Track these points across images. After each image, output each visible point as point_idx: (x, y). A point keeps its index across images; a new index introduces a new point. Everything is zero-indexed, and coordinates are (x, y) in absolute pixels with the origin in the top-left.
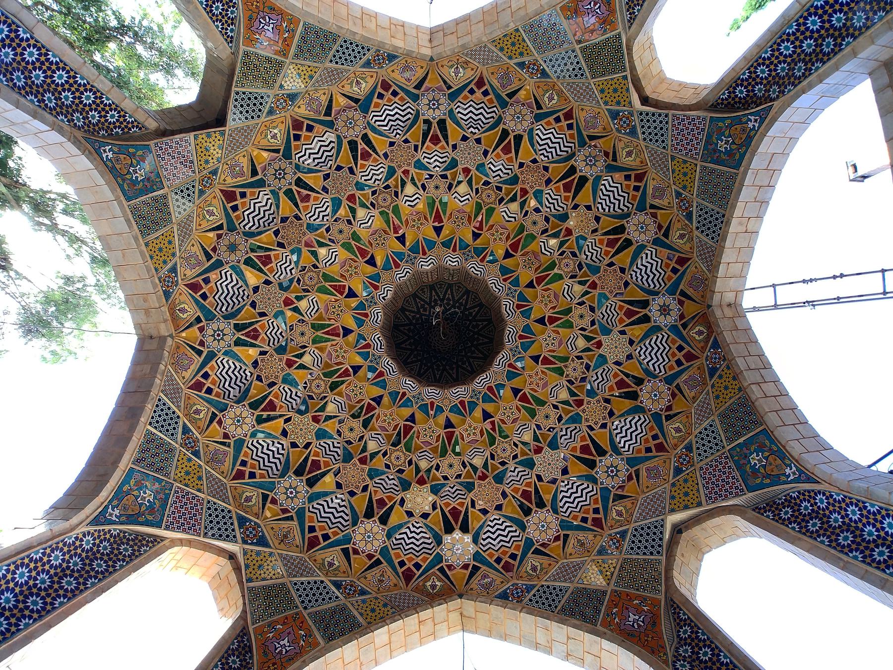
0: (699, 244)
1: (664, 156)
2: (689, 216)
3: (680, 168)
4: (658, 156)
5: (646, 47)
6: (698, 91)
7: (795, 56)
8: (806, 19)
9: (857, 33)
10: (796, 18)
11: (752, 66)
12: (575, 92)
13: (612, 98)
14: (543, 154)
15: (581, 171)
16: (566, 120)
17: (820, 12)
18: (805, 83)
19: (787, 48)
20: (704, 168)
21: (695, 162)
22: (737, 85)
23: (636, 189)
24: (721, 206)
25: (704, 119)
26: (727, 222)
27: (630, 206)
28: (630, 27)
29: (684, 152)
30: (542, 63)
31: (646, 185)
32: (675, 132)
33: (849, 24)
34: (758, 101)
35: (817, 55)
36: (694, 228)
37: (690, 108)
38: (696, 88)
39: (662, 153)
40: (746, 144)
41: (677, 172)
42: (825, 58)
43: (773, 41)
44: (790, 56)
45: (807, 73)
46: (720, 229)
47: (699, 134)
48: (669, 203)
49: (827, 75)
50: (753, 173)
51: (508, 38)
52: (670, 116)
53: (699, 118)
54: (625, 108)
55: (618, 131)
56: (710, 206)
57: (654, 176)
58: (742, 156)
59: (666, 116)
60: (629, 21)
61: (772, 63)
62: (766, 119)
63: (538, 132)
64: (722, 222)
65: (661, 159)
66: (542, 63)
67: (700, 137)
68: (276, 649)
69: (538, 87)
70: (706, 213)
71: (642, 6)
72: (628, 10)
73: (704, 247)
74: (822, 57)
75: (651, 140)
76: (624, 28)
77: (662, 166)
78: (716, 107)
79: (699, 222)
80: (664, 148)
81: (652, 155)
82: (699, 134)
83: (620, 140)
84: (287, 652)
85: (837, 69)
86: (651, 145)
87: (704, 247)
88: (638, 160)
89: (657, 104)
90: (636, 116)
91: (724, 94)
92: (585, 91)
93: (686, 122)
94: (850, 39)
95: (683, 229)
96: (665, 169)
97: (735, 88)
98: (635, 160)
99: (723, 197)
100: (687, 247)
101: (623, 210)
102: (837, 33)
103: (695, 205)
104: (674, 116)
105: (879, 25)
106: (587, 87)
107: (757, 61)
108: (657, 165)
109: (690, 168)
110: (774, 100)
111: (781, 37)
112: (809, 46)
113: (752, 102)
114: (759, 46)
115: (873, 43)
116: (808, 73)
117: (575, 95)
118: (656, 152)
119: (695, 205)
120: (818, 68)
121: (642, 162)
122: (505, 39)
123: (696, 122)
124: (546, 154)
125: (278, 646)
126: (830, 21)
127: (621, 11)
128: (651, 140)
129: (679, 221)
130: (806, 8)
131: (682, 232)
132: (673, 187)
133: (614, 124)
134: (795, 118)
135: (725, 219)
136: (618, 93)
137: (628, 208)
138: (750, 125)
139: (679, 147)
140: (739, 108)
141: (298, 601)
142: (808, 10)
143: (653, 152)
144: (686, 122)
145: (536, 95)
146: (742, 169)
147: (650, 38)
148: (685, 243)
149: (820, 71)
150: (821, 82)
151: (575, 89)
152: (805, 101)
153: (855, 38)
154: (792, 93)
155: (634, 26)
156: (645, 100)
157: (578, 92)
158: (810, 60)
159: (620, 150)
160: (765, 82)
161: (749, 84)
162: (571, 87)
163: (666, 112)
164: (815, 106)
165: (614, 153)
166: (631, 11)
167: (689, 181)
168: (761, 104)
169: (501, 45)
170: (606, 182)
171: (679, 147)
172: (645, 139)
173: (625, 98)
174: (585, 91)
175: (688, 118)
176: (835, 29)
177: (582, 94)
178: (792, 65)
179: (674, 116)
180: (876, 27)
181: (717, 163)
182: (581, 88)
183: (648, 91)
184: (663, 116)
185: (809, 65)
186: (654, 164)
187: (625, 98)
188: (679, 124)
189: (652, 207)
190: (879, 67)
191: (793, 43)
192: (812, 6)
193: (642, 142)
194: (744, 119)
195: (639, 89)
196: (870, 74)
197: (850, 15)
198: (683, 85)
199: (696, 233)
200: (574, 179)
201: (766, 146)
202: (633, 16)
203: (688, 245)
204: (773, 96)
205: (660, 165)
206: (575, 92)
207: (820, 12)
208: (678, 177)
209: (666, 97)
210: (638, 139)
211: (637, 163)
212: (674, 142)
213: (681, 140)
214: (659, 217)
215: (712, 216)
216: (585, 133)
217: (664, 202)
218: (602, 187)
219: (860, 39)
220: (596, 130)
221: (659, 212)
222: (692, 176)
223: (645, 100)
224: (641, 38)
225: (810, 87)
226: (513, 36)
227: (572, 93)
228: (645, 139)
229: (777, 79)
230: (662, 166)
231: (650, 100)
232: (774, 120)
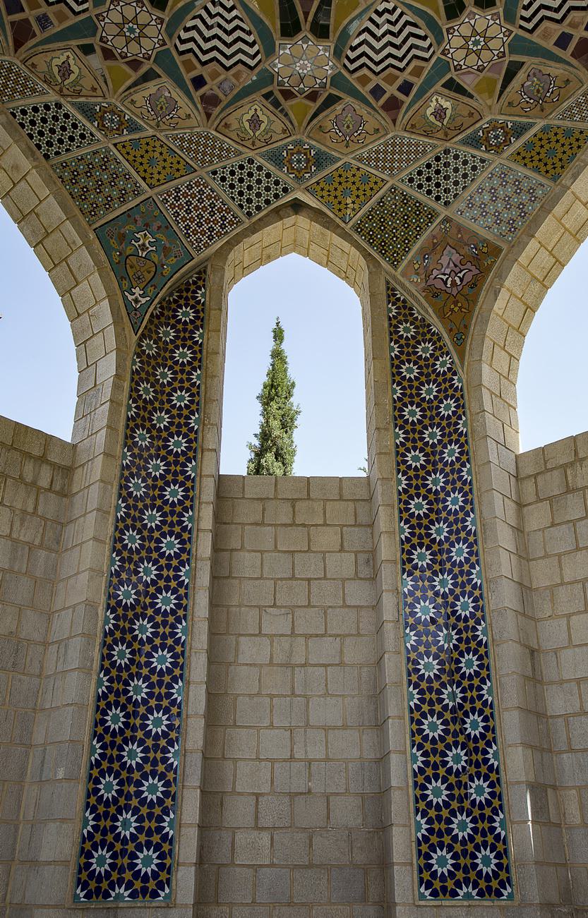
0: (30, 84)
1: (203, 161)
2: (87, 111)
3: (167, 164)
4: (212, 155)
5: (350, 271)
6: (239, 270)
7: (165, 398)
8: (175, 656)
9: (126, 473)
10: (200, 434)
11: (201, 351)
12: (405, 149)
13: (342, 180)
14: (391, 12)
15: (305, 40)
16: (393, 98)
17: (171, 619)
18: (127, 385)
19: (181, 399)
20: (137, 192)
21: (157, 190)
22: (197, 318)
23: (199, 82)
24: (64, 166)
25: (199, 249)
26: (33, 154)
27: (182, 48)
28: (388, 283)
29: (183, 189)
30: (485, 156)
31: (191, 98)
32: (218, 204)
33: (143, 473)
34: (156, 321)
35: (143, 419)
36: (62, 101)
37: (230, 245)
38: (246, 270)
39: (211, 162)
40: (122, 270)
41: (165, 156)
42: (132, 424)
43: (202, 394)
44: (170, 395)
45: (134, 395)
46: (31, 136)
47: (188, 227)
48: (133, 102)
49: (113, 412)
50: (74, 242)
51: (565, 157)
52: (244, 218)
53: (207, 246)
54: (314, 180)
55: (299, 143)
56: (77, 153)
57: (192, 122)
58: (107, 250)
59: (249, 214)
60: (393, 289)
61: (182, 371)
62: (128, 314)
63: (425, 44)
64: (39, 147)
65: (204, 154)
66: (485, 156)
67: (182, 225)
68: (445, 283)
69: (471, 115)
70: (72, 139)
71: (390, 319)
72: (404, 301)
73: (19, 88)
74: (139, 420)
75: (242, 167)
76: (394, 278)
77: (193, 147)
78: (199, 273)
79: (66, 116)
80: (215, 173)
81: (221, 149)
82: (188, 227)
83: (284, 131)
84: (461, 280)
85: (109, 427)
86: (235, 161)
87: (19, 88)
88: (235, 126)
89: (278, 214)
90: (289, 181)
91: (204, 295)
92: (393, 161)
93: (217, 228)
94: (137, 366)
95: (76, 83)
96: (186, 144)
97: (197, 312)
98: (240, 120)
99: (74, 180)
100: (40, 61)
101: (187, 30)
102: (145, 454)
103: (98, 135)
104: (240, 222)
105: (114, 502)
106: (392, 169)
107: (200, 361)
108: (202, 141)
109: (156, 176)
110: (140, 339)
111: (198, 404)
112: (160, 420)
113: (162, 314)
114: (216, 378)
115: (102, 481)
116: (134, 395)
117: (402, 145)
118: (220, 157)
119: (98, 135)
120: (129, 408)
121: (227, 126)
122: (569, 153)
123: (205, 239)
124: (386, 16)
125: (445, 278)
126: (146, 679)
127: (413, 295)
128: (242, 167)
129: (94, 89)
130: (199, 451)
131: (73, 77)
132: (151, 132)
133: (311, 147)
134: (98, 340)
135: (39, 154)
136: (335, 190)
137: (183, 42)
138: (137, 291)
139: (195, 190)
140: (171, 294)
141: (429, 202)
142: (195, 451)
143: (224, 153)
144: (217, 228)
145: (466, 99)
146: (92, 236)
147: (353, 284)
148: (49, 66)
149: (123, 410)
150: (111, 400)
151: (408, 153)
152: (108, 368)
153: (123, 468)
154: (129, 363)
155: (383, 287)
156: (297, 206)
157: (401, 153)
158: (145, 409)
159: (273, 118)
160: (171, 347)
161: (185, 330)
162: (417, 152)
163: (254, 219)
164: (92, 369)
165: (276, 104)
166: (400, 304)
167: (139, 160)
168: (150, 321)
169: (573, 140)
170: (252, 51)
171: (195, 190)
172: (251, 161)
173: (325, 193)
174: (393, 161)
175: (219, 235)
176: (137, 616)
177: (393, 153)
178: (158, 387)
179: (240, 222)
180: (114, 496)
181: (128, 214)
182: (400, 161)
183: (302, 221)
184: (253, 211)
185: (141, 403)
186: (207, 138)
187: (325, 193)
188: (224, 218)
189: (149, 76)
190: (73, 462)
191: (173, 504)
192: (195, 458)
193: (251, 154)
194: (150, 290)
195: (317, 215)
196: (74, 447)
197: (150, 482)
198: (266, 258)
199: (52, 97)
200: (306, 14)
201: (94, 286)
202: (393, 299)
203: (42, 67)
204: (146, 342)
205: (198, 143)
206: (405, 149)
207: (167, 679)
208: (159, 150)
209: (271, 232)
210: (262, 156)
211: (232, 120)
212: (207, 191)
213: (201, 201)
214: (126, 68)
215: (61, 141)
216: (348, 99)
217: (140, 96)
218: (250, 39)
219: (117, 472)
220: (332, 117)
221: (134, 76)
222: (141, 169)
223: (297, 206)
224: (364, 276)
225: (116, 387)
226: (559, 164)
227: (409, 145)
228: (251, 161)
229: (160, 360)
230: (193, 147)
231: (290, 211)
232: (117, 321)
